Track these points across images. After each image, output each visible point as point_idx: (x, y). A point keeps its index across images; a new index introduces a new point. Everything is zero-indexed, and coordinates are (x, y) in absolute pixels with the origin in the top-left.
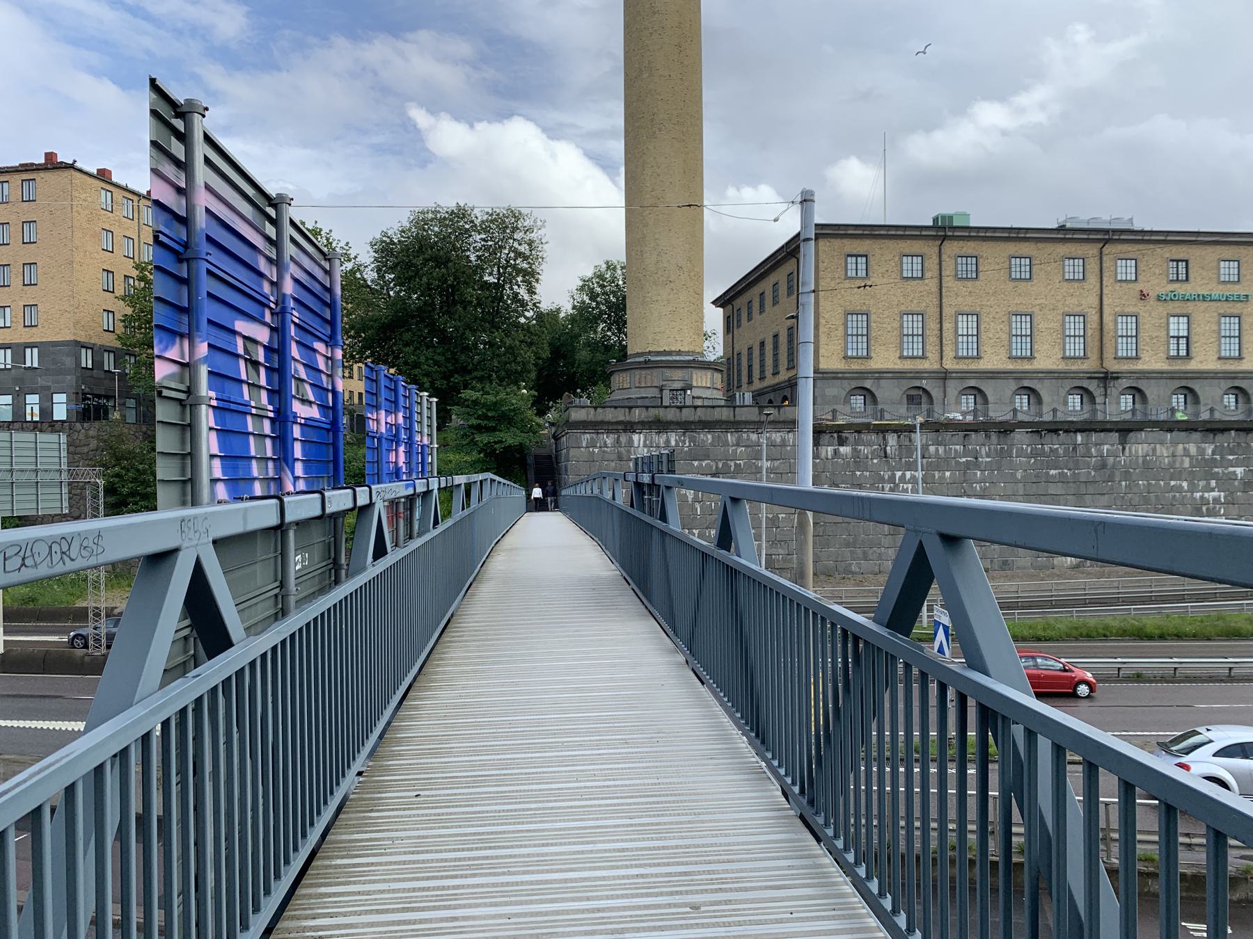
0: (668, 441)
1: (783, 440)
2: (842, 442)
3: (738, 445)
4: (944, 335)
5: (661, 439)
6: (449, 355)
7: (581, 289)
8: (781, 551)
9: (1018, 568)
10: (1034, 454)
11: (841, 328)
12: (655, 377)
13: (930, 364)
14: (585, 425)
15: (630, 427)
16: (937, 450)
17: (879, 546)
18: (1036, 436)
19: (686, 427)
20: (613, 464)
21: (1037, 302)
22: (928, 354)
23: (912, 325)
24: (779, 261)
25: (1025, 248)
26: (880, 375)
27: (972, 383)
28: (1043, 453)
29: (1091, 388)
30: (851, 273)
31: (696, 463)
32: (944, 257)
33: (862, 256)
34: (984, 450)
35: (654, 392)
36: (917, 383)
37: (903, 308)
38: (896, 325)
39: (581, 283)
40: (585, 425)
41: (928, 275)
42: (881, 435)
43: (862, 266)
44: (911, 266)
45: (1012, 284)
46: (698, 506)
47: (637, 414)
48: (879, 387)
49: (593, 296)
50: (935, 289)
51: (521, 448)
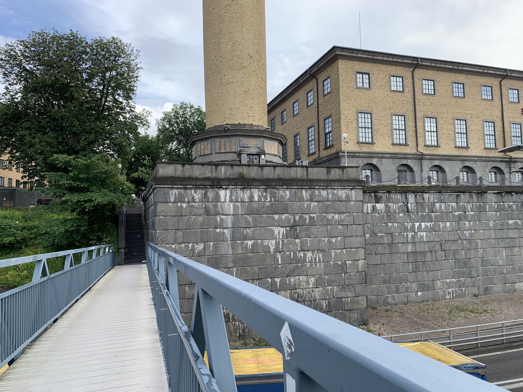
0: (251, 197)
1: (347, 196)
2: (378, 200)
3: (311, 200)
4: (418, 130)
5: (245, 195)
6: (60, 139)
7: (164, 119)
8: (349, 294)
9: (495, 292)
10: (498, 210)
11: (355, 122)
12: (232, 144)
13: (410, 150)
14: (173, 181)
15: (217, 183)
16: (441, 206)
17: (407, 281)
18: (499, 196)
19: (268, 184)
20: (201, 219)
21: (469, 112)
22: (408, 143)
23: (398, 123)
24: (300, 85)
25: (461, 78)
26: (382, 156)
27: (437, 163)
28: (504, 209)
29: (502, 168)
30: (360, 85)
31: (276, 217)
32: (415, 79)
33: (366, 74)
34: (469, 206)
35: (234, 157)
36: (404, 162)
37: (393, 111)
38: (389, 122)
39: (163, 116)
40: (173, 181)
41: (406, 90)
42: (404, 195)
43: (366, 81)
44: (396, 84)
45: (454, 100)
46: (279, 256)
47: (223, 172)
48: (381, 163)
49: (169, 122)
50: (411, 100)
51: (112, 207)
